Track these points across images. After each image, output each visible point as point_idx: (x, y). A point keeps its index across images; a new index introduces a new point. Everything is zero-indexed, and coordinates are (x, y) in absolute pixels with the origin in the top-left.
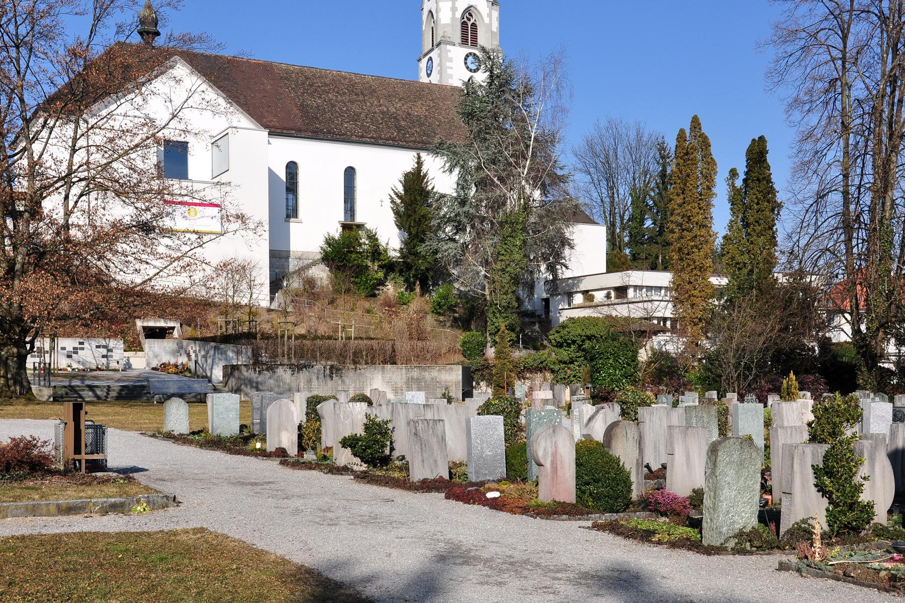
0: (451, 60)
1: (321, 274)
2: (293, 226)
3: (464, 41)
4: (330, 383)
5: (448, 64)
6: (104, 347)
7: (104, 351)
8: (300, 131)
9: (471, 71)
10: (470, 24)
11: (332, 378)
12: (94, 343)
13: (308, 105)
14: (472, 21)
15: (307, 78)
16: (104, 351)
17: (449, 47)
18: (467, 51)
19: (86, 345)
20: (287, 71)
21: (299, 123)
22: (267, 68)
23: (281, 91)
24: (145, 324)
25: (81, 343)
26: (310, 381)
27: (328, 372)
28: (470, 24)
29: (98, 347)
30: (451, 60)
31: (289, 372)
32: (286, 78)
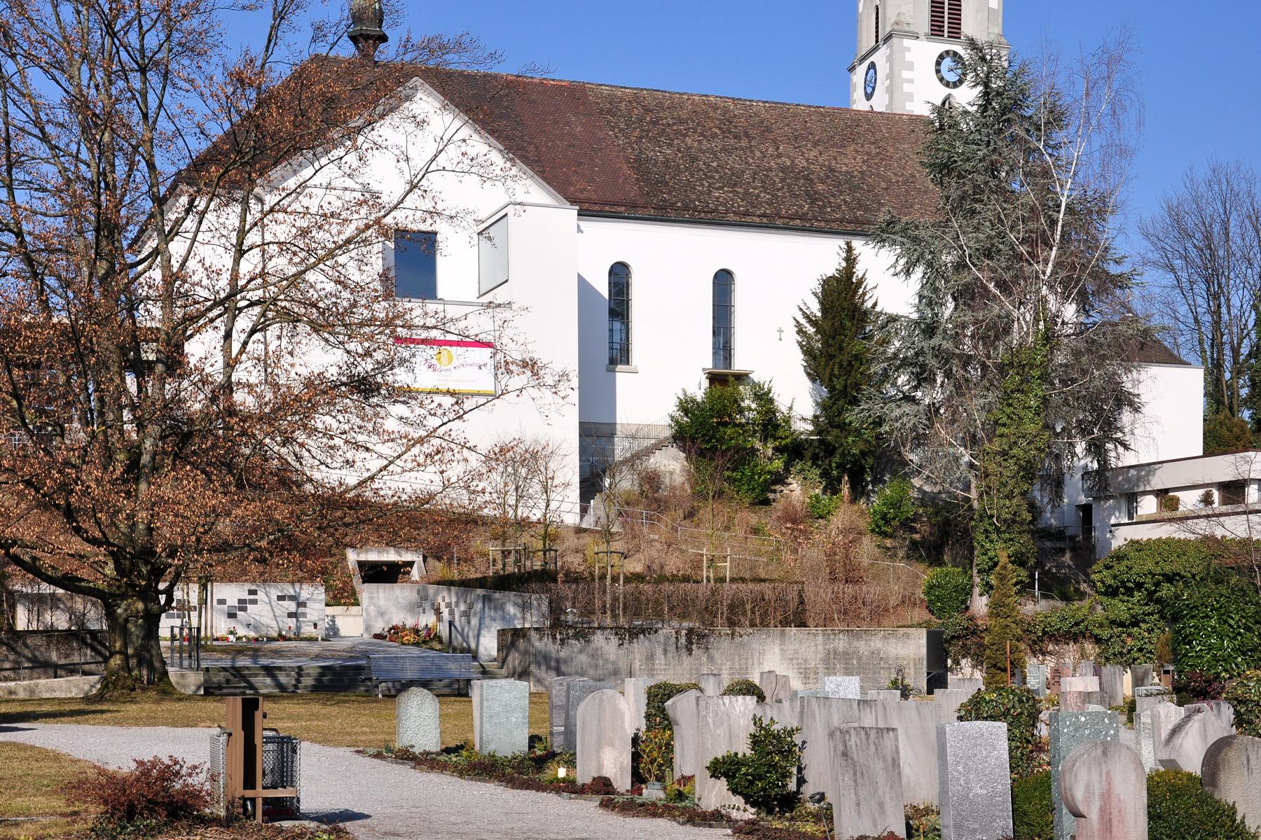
0: (910, 67)
1: (672, 465)
2: (622, 378)
3: (936, 30)
4: (687, 661)
5: (906, 74)
6: (292, 598)
7: (291, 606)
8: (634, 206)
9: (947, 84)
11: (690, 651)
12: (274, 592)
13: (648, 160)
15: (647, 110)
16: (291, 606)
17: (907, 42)
18: (941, 47)
19: (261, 596)
20: (611, 99)
21: (632, 192)
22: (575, 94)
23: (600, 134)
24: (363, 557)
25: (252, 592)
26: (651, 657)
27: (683, 640)
29: (281, 598)
30: (910, 67)
31: (614, 641)
32: (609, 112)
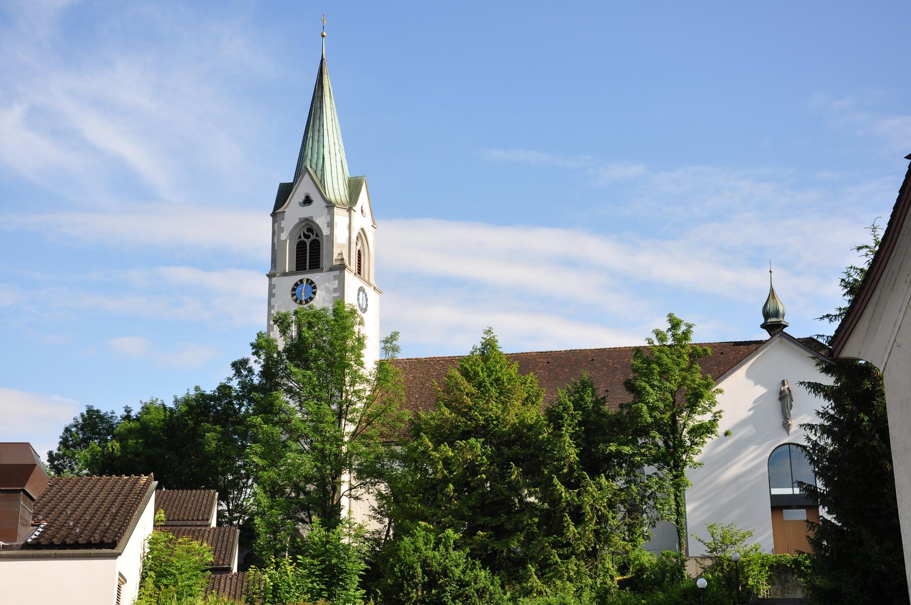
10: (308, 242)
14: (313, 237)
28: (308, 242)
